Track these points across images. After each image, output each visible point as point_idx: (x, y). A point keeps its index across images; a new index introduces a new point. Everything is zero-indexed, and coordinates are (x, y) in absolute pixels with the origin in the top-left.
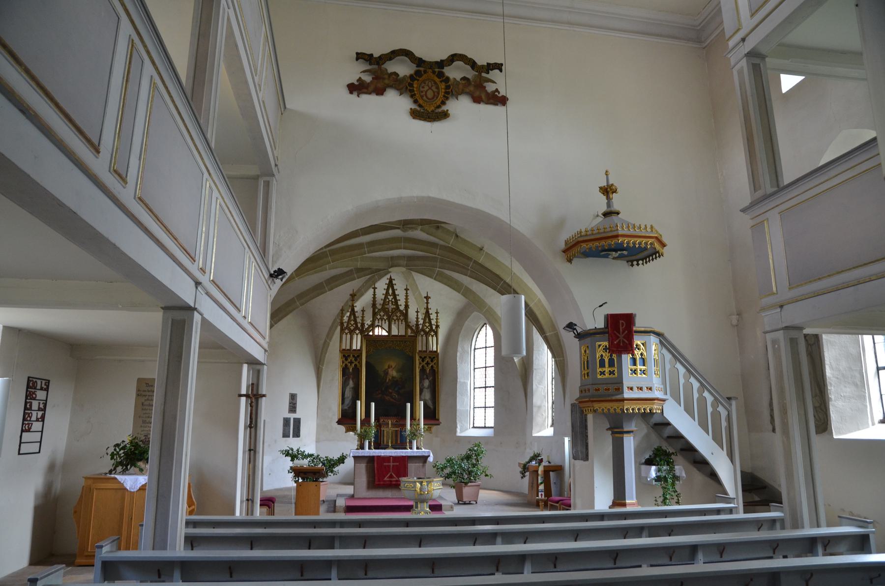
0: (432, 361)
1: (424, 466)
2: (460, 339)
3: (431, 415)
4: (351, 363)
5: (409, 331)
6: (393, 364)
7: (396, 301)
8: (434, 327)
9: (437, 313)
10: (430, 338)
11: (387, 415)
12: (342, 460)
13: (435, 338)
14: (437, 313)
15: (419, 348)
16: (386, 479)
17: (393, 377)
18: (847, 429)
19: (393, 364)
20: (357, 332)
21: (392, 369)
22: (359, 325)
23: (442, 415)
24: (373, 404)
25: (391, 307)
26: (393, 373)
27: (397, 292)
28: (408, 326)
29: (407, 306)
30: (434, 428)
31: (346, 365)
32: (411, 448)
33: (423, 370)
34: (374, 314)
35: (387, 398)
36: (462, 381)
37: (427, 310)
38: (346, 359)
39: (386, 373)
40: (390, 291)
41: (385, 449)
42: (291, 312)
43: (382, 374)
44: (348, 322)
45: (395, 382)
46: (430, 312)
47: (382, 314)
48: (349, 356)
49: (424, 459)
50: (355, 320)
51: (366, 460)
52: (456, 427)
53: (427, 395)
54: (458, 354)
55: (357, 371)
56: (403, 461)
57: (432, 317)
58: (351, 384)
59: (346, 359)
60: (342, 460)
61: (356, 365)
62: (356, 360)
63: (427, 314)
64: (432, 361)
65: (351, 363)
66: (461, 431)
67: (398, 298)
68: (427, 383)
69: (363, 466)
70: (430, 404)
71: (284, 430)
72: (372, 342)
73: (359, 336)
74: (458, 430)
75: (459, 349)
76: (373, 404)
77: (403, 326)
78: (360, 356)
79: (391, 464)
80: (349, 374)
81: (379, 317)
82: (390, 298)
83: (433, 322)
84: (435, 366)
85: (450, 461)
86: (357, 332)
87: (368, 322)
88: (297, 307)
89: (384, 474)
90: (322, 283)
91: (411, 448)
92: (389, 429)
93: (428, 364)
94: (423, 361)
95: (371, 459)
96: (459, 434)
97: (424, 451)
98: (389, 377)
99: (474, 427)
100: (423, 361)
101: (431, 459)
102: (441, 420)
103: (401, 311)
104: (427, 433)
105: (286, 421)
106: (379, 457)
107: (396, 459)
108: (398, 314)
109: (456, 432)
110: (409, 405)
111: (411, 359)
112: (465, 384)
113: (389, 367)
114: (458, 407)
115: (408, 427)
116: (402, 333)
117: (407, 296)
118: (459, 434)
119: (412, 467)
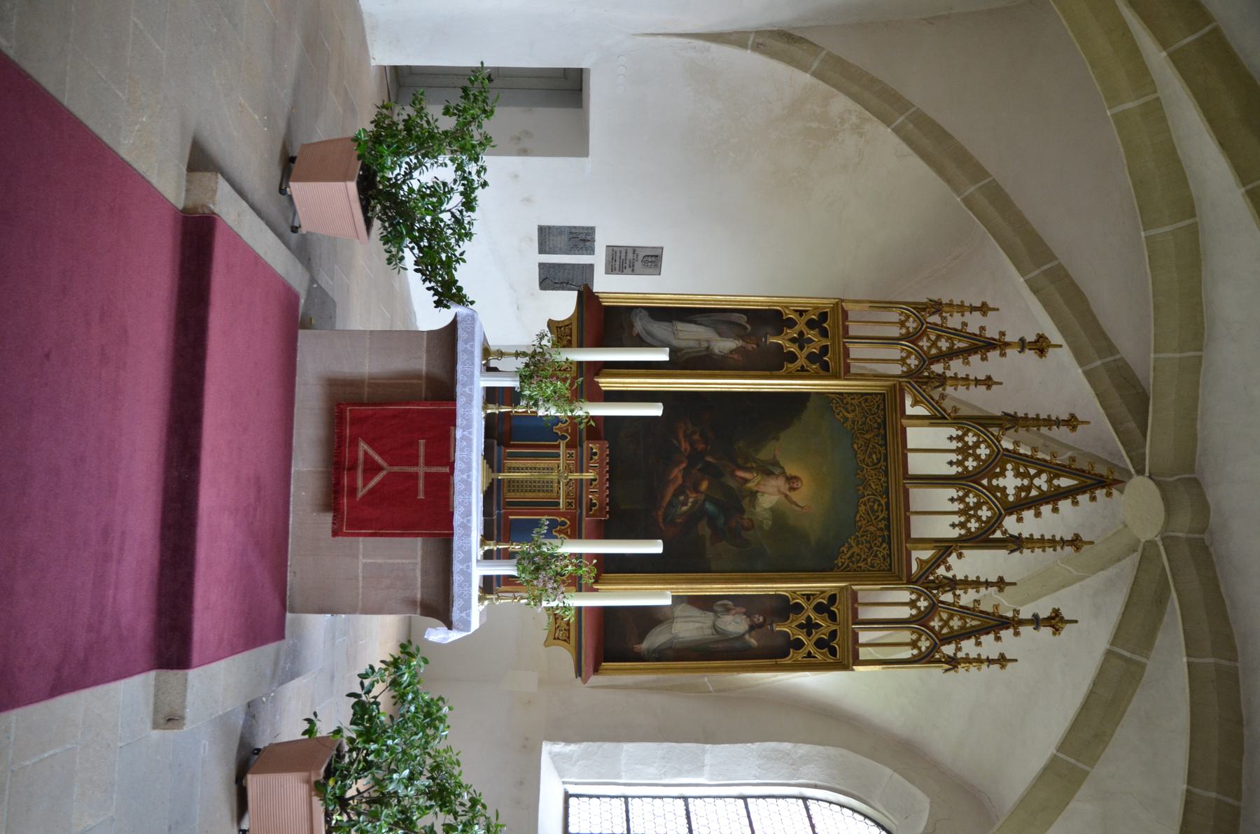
0: (820, 644)
1: (411, 604)
2: (832, 751)
3: (614, 641)
4: (801, 341)
5: (926, 554)
6: (802, 496)
7: (1034, 504)
8: (949, 650)
9: (1002, 660)
10: (906, 636)
11: (616, 471)
12: (448, 293)
13: (907, 653)
14: (1002, 660)
15: (866, 592)
16: (363, 447)
17: (753, 495)
18: (576, 293)
19: (802, 496)
20: (913, 362)
21: (785, 489)
22: (938, 368)
23: (620, 685)
24: (656, 410)
25: (1010, 482)
26: (769, 495)
27: (1065, 505)
28: (945, 548)
29: (1016, 543)
30: (564, 656)
31: (791, 323)
32: (488, 556)
33: (784, 608)
34: (983, 422)
35: (677, 473)
36: (708, 759)
37: (1013, 623)
38: (811, 324)
39: (768, 470)
40: (1065, 482)
41: (488, 455)
42: (940, 171)
43: (764, 455)
44: (942, 330)
45: (734, 502)
46: (1006, 634)
47: (983, 451)
48: (824, 333)
49: (439, 606)
50: (952, 354)
51: (439, 371)
52: (568, 740)
53: (690, 628)
54: (787, 746)
55: (774, 363)
56: (435, 520)
57: (988, 639)
58: (725, 345)
59: (811, 324)
60: (448, 293)
61: (792, 357)
62: (811, 358)
63: (997, 623)
64: (820, 644)
65: (801, 341)
66: (554, 757)
67: (1046, 509)
68: (735, 624)
69: (420, 363)
70: (656, 639)
71: (560, 230)
72: (877, 423)
73: (897, 369)
74: (559, 747)
75: (803, 749)
76: (656, 410)
77: (944, 528)
78: (826, 371)
79: (421, 470)
80: (759, 332)
81: (970, 439)
82: (1041, 482)
83: (968, 647)
84: (799, 656)
85: (431, 717)
86: (913, 362)
87: (956, 395)
88: (957, 190)
89: (386, 452)
90: (1051, 256)
91: (488, 556)
92: (559, 473)
93: (809, 626)
94: (819, 608)
95: (442, 390)
96: (547, 748)
97: (474, 611)
98: (753, 480)
99: (567, 796)
100: (819, 608)
101: (437, 635)
102: (595, 680)
103: (996, 522)
104: (545, 621)
105: (581, 239)
106: (451, 418)
107: (442, 488)
108: (985, 513)
109: (553, 739)
110: (655, 548)
111: (823, 566)
112: (699, 768)
113: (790, 479)
114: (628, 747)
115: (569, 548)
116: (923, 528)
117: (1053, 543)
118: (547, 748)
119: (406, 555)
